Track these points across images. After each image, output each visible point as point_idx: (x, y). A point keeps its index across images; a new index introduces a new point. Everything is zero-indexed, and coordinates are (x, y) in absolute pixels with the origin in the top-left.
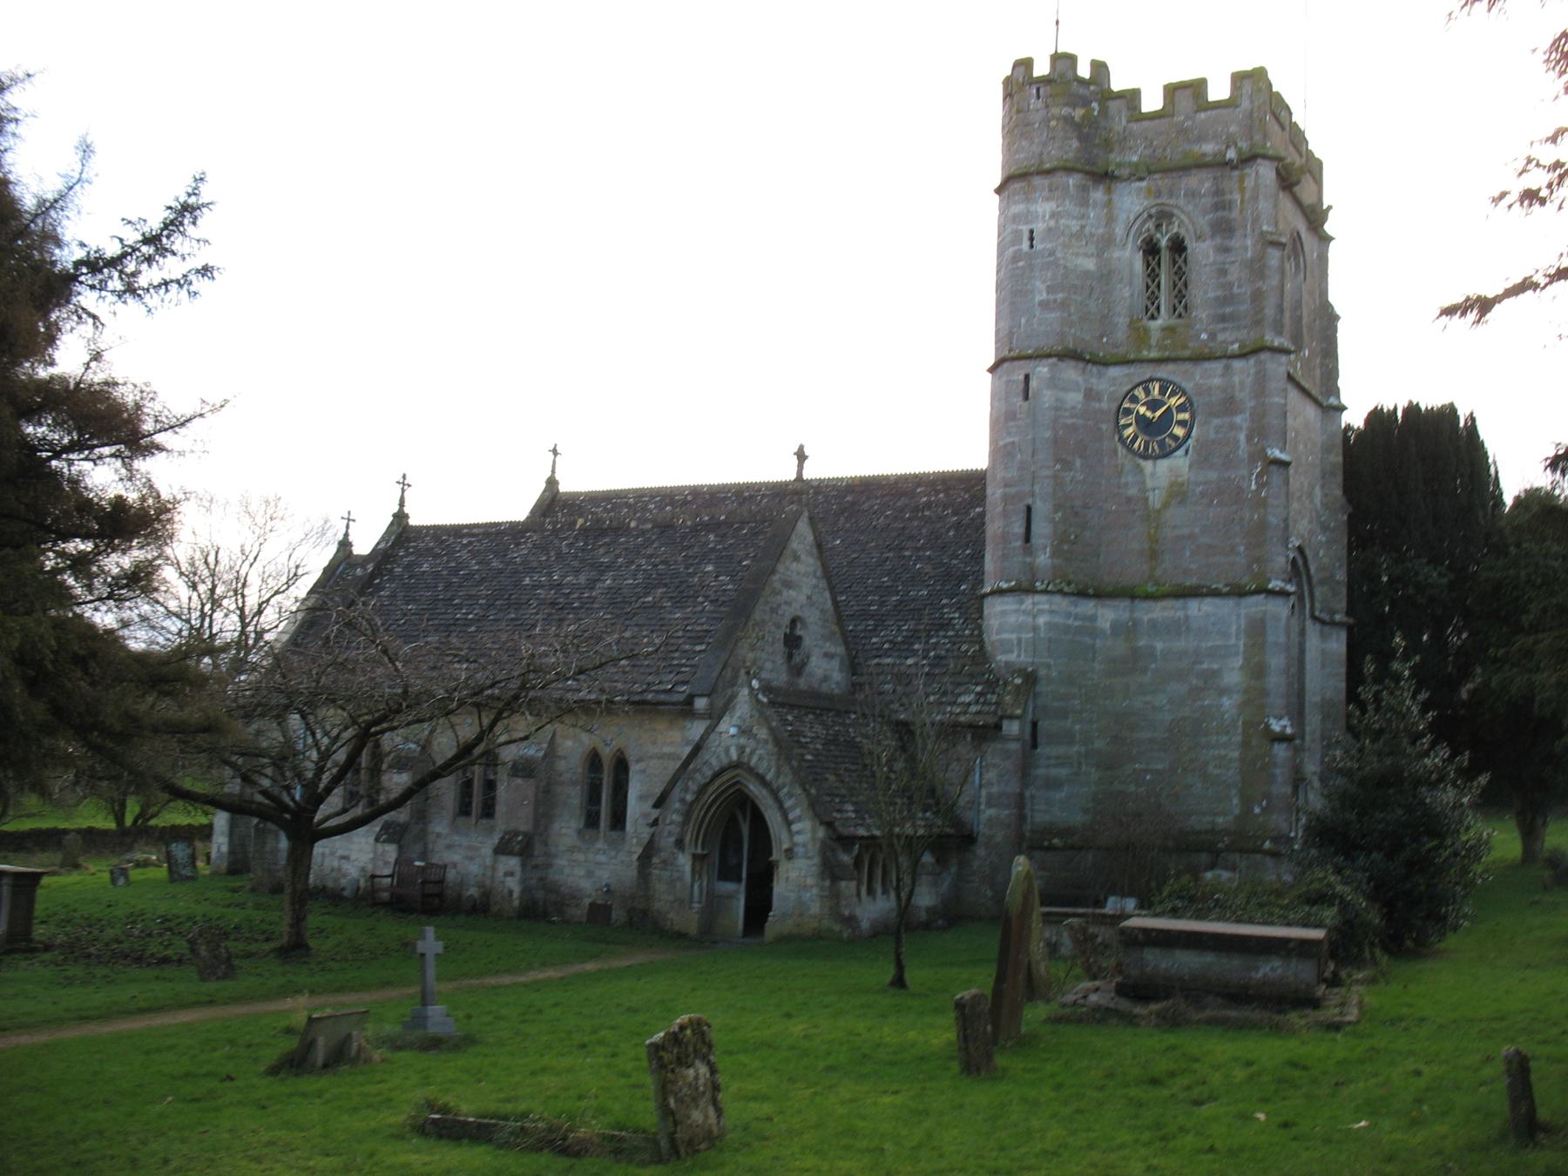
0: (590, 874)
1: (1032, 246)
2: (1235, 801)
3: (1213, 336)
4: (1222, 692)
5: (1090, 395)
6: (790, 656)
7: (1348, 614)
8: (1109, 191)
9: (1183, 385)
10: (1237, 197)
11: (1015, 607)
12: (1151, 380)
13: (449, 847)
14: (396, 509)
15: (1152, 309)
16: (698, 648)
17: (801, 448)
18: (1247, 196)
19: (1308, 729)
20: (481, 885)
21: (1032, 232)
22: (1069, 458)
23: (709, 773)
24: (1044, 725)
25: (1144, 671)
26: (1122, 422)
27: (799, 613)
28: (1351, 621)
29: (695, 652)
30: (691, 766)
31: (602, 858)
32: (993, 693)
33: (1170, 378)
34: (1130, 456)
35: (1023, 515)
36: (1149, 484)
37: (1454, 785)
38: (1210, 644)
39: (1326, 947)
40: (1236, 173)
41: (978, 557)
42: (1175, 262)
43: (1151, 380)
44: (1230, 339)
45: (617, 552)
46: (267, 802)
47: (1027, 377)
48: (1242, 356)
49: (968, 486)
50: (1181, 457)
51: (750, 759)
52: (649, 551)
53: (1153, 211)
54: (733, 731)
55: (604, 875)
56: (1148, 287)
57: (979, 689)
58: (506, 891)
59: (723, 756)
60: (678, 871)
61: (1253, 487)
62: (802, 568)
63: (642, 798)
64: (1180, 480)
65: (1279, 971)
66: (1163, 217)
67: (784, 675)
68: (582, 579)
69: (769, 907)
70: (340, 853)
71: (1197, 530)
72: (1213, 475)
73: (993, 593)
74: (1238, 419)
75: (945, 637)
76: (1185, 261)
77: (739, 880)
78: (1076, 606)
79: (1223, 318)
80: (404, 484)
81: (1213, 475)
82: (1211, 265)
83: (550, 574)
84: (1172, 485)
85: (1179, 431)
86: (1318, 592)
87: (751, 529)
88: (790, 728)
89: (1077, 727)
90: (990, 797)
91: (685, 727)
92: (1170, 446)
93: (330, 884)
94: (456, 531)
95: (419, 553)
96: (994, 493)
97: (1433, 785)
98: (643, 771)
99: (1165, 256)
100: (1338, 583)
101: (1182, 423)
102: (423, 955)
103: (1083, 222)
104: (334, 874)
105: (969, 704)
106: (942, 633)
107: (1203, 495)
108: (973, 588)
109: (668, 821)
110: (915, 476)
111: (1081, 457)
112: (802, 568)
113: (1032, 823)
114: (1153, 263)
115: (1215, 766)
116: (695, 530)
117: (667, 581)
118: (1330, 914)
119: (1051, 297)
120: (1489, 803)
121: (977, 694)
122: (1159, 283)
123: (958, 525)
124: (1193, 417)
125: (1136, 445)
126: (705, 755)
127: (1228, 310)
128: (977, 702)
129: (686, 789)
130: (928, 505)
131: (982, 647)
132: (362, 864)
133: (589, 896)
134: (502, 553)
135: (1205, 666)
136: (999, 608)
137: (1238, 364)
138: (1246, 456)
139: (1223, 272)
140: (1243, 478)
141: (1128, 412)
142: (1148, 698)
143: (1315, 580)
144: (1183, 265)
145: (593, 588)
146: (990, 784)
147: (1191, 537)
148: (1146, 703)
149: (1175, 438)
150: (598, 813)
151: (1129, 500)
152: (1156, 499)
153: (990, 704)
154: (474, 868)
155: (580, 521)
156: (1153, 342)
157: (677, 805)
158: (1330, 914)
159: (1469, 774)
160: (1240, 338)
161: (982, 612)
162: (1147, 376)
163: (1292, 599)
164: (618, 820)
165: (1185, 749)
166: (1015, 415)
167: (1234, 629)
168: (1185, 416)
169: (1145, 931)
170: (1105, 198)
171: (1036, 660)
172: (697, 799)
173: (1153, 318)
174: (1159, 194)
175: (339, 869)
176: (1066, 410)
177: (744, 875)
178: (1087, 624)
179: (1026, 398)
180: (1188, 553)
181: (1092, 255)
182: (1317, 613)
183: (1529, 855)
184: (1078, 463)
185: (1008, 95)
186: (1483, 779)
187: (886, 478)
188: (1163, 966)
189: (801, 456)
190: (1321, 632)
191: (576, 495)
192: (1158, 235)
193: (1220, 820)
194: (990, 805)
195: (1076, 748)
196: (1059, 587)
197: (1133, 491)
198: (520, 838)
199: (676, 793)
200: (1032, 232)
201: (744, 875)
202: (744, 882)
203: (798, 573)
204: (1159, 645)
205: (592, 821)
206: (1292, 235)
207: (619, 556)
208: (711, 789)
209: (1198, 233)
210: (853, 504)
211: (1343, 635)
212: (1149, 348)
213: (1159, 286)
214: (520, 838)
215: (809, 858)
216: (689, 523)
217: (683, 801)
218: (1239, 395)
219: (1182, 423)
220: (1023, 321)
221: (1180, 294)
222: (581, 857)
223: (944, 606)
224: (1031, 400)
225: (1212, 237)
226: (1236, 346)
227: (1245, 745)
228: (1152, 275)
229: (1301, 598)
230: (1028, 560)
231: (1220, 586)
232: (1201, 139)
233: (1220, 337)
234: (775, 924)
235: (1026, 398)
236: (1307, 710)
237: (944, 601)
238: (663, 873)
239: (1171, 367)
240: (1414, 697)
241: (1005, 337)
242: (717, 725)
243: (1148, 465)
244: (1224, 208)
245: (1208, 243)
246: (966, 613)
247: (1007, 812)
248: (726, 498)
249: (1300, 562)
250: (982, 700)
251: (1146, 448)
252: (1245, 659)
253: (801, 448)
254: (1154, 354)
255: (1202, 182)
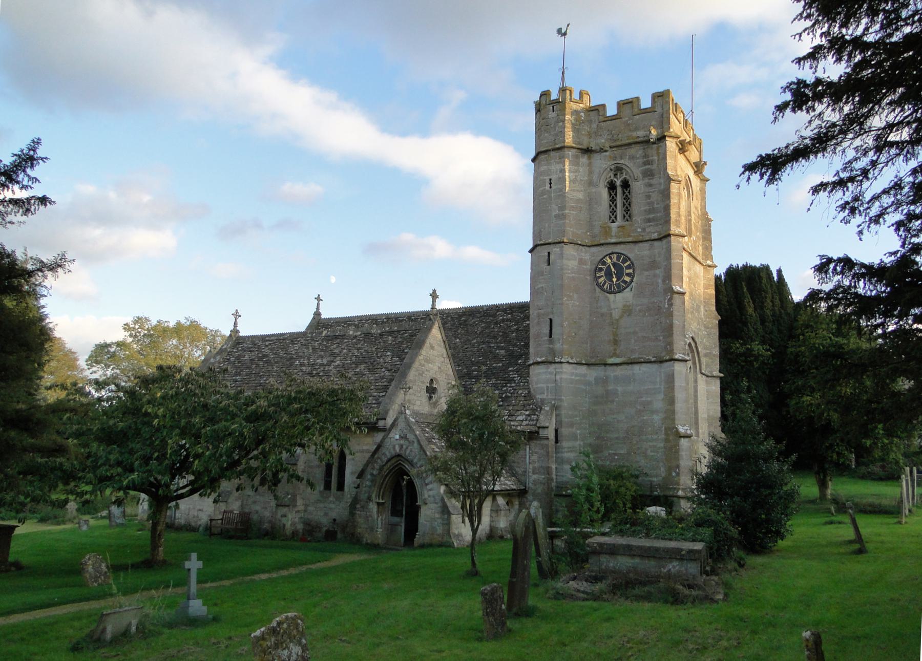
0: (326, 514)
1: (551, 187)
2: (662, 469)
3: (644, 230)
4: (653, 412)
5: (581, 262)
6: (430, 398)
7: (720, 372)
8: (589, 158)
9: (629, 255)
10: (656, 158)
11: (546, 371)
12: (613, 253)
13: (255, 502)
14: (232, 328)
15: (613, 217)
16: (381, 394)
17: (434, 291)
18: (661, 157)
19: (700, 431)
20: (270, 522)
21: (551, 180)
22: (571, 294)
23: (385, 459)
24: (564, 431)
25: (612, 401)
26: (598, 275)
27: (434, 376)
28: (722, 375)
29: (379, 396)
30: (376, 456)
31: (332, 506)
32: (535, 415)
33: (622, 252)
34: (602, 292)
35: (548, 323)
36: (613, 306)
37: (778, 460)
38: (646, 388)
39: (704, 553)
40: (655, 146)
41: (527, 345)
42: (624, 193)
43: (613, 253)
44: (653, 231)
45: (343, 347)
46: (155, 482)
47: (549, 253)
48: (660, 239)
49: (522, 308)
50: (628, 292)
51: (405, 452)
52: (359, 346)
53: (612, 167)
54: (397, 437)
55: (333, 515)
56: (610, 206)
57: (527, 413)
58: (282, 525)
59: (392, 450)
60: (369, 512)
61: (666, 306)
62: (435, 353)
63: (352, 473)
64: (628, 303)
65: (677, 568)
66: (618, 170)
67: (427, 407)
68: (325, 361)
69: (417, 530)
70: (198, 507)
71: (637, 329)
72: (645, 301)
73: (534, 364)
74: (657, 272)
75: (510, 387)
76: (629, 192)
77: (402, 516)
78: (576, 370)
79: (649, 220)
80: (237, 315)
81: (645, 301)
82: (643, 193)
83: (309, 359)
84: (624, 306)
85: (627, 279)
86: (703, 360)
87: (410, 333)
88: (427, 435)
89: (578, 432)
90: (534, 469)
91: (374, 436)
92: (623, 286)
93: (193, 524)
94: (264, 338)
95: (244, 350)
96: (533, 313)
97: (766, 460)
98: (353, 459)
99: (619, 190)
100: (714, 355)
101: (628, 275)
102: (189, 570)
103: (577, 174)
104: (195, 519)
105: (522, 421)
106: (509, 385)
107: (640, 311)
108: (525, 362)
109: (364, 485)
110: (496, 306)
111: (577, 293)
112: (435, 353)
113: (557, 482)
114: (613, 194)
115: (651, 451)
116: (381, 335)
117: (367, 361)
118: (707, 532)
119: (560, 212)
120: (800, 467)
121: (527, 415)
122: (616, 204)
123: (517, 330)
124: (634, 271)
125: (605, 287)
126: (383, 450)
127: (651, 216)
128: (526, 420)
129: (373, 469)
130: (503, 321)
131: (529, 392)
132: (210, 513)
133: (326, 526)
134: (285, 348)
135: (644, 399)
136: (537, 371)
137: (656, 243)
138: (662, 291)
139: (649, 197)
140: (661, 302)
141: (601, 270)
142: (615, 416)
143: (701, 354)
144: (628, 194)
145: (330, 365)
146: (534, 462)
147: (635, 333)
148: (614, 418)
149: (625, 282)
150: (330, 482)
151: (602, 315)
152: (616, 314)
153: (533, 420)
154: (267, 514)
155: (325, 332)
156: (613, 234)
157: (369, 477)
158: (707, 532)
159: (785, 454)
160: (658, 230)
161: (529, 374)
162: (610, 252)
163: (690, 364)
164: (341, 487)
165: (635, 442)
166: (543, 272)
167: (658, 380)
168: (630, 271)
169: (601, 545)
170: (587, 162)
171: (557, 397)
172: (379, 473)
173: (613, 222)
174: (615, 158)
175: (198, 517)
176: (569, 270)
177: (404, 513)
178: (582, 378)
179: (549, 264)
180: (633, 341)
181: (582, 191)
182: (703, 371)
183: (823, 496)
184: (576, 296)
185: (538, 111)
186: (794, 457)
187: (482, 307)
188: (612, 565)
189: (434, 295)
190: (706, 381)
191: (330, 319)
192: (615, 180)
193: (655, 479)
194: (534, 473)
195: (578, 443)
196: (567, 360)
197: (604, 310)
198: (289, 496)
199: (369, 470)
200: (551, 180)
201: (404, 513)
202: (404, 517)
203: (433, 356)
204: (620, 389)
205: (328, 486)
206: (685, 177)
207: (344, 349)
208: (385, 468)
209: (636, 177)
210: (465, 321)
211: (718, 382)
212: (611, 237)
213: (616, 206)
214: (289, 496)
215: (436, 503)
216: (379, 331)
217: (372, 474)
218: (657, 259)
219: (628, 275)
220: (547, 225)
221: (627, 210)
222: (322, 505)
223: (511, 371)
224: (551, 265)
225: (643, 180)
226: (656, 234)
227: (667, 440)
228: (613, 200)
229: (694, 363)
230: (551, 346)
231: (650, 357)
232: (636, 129)
233: (648, 230)
234: (418, 539)
235: (549, 264)
236: (700, 421)
237: (510, 369)
238: (362, 513)
239: (623, 246)
240: (754, 413)
241: (536, 234)
242: (388, 434)
243: (611, 296)
244: (649, 164)
245: (641, 182)
246: (521, 374)
247: (543, 477)
248: (403, 320)
249: (693, 345)
250: (529, 418)
251: (610, 288)
252: (665, 395)
253: (434, 291)
254: (613, 240)
255: (637, 151)
